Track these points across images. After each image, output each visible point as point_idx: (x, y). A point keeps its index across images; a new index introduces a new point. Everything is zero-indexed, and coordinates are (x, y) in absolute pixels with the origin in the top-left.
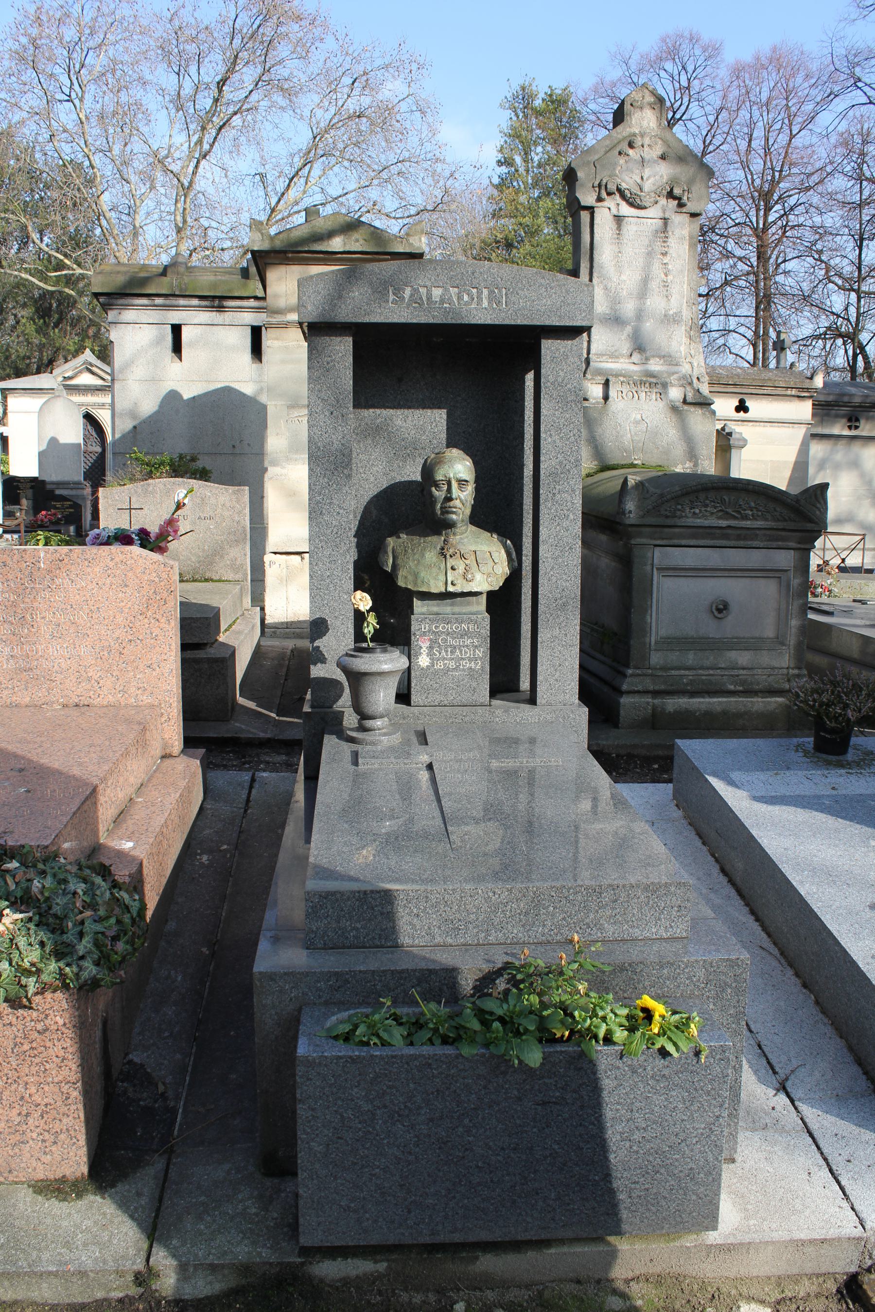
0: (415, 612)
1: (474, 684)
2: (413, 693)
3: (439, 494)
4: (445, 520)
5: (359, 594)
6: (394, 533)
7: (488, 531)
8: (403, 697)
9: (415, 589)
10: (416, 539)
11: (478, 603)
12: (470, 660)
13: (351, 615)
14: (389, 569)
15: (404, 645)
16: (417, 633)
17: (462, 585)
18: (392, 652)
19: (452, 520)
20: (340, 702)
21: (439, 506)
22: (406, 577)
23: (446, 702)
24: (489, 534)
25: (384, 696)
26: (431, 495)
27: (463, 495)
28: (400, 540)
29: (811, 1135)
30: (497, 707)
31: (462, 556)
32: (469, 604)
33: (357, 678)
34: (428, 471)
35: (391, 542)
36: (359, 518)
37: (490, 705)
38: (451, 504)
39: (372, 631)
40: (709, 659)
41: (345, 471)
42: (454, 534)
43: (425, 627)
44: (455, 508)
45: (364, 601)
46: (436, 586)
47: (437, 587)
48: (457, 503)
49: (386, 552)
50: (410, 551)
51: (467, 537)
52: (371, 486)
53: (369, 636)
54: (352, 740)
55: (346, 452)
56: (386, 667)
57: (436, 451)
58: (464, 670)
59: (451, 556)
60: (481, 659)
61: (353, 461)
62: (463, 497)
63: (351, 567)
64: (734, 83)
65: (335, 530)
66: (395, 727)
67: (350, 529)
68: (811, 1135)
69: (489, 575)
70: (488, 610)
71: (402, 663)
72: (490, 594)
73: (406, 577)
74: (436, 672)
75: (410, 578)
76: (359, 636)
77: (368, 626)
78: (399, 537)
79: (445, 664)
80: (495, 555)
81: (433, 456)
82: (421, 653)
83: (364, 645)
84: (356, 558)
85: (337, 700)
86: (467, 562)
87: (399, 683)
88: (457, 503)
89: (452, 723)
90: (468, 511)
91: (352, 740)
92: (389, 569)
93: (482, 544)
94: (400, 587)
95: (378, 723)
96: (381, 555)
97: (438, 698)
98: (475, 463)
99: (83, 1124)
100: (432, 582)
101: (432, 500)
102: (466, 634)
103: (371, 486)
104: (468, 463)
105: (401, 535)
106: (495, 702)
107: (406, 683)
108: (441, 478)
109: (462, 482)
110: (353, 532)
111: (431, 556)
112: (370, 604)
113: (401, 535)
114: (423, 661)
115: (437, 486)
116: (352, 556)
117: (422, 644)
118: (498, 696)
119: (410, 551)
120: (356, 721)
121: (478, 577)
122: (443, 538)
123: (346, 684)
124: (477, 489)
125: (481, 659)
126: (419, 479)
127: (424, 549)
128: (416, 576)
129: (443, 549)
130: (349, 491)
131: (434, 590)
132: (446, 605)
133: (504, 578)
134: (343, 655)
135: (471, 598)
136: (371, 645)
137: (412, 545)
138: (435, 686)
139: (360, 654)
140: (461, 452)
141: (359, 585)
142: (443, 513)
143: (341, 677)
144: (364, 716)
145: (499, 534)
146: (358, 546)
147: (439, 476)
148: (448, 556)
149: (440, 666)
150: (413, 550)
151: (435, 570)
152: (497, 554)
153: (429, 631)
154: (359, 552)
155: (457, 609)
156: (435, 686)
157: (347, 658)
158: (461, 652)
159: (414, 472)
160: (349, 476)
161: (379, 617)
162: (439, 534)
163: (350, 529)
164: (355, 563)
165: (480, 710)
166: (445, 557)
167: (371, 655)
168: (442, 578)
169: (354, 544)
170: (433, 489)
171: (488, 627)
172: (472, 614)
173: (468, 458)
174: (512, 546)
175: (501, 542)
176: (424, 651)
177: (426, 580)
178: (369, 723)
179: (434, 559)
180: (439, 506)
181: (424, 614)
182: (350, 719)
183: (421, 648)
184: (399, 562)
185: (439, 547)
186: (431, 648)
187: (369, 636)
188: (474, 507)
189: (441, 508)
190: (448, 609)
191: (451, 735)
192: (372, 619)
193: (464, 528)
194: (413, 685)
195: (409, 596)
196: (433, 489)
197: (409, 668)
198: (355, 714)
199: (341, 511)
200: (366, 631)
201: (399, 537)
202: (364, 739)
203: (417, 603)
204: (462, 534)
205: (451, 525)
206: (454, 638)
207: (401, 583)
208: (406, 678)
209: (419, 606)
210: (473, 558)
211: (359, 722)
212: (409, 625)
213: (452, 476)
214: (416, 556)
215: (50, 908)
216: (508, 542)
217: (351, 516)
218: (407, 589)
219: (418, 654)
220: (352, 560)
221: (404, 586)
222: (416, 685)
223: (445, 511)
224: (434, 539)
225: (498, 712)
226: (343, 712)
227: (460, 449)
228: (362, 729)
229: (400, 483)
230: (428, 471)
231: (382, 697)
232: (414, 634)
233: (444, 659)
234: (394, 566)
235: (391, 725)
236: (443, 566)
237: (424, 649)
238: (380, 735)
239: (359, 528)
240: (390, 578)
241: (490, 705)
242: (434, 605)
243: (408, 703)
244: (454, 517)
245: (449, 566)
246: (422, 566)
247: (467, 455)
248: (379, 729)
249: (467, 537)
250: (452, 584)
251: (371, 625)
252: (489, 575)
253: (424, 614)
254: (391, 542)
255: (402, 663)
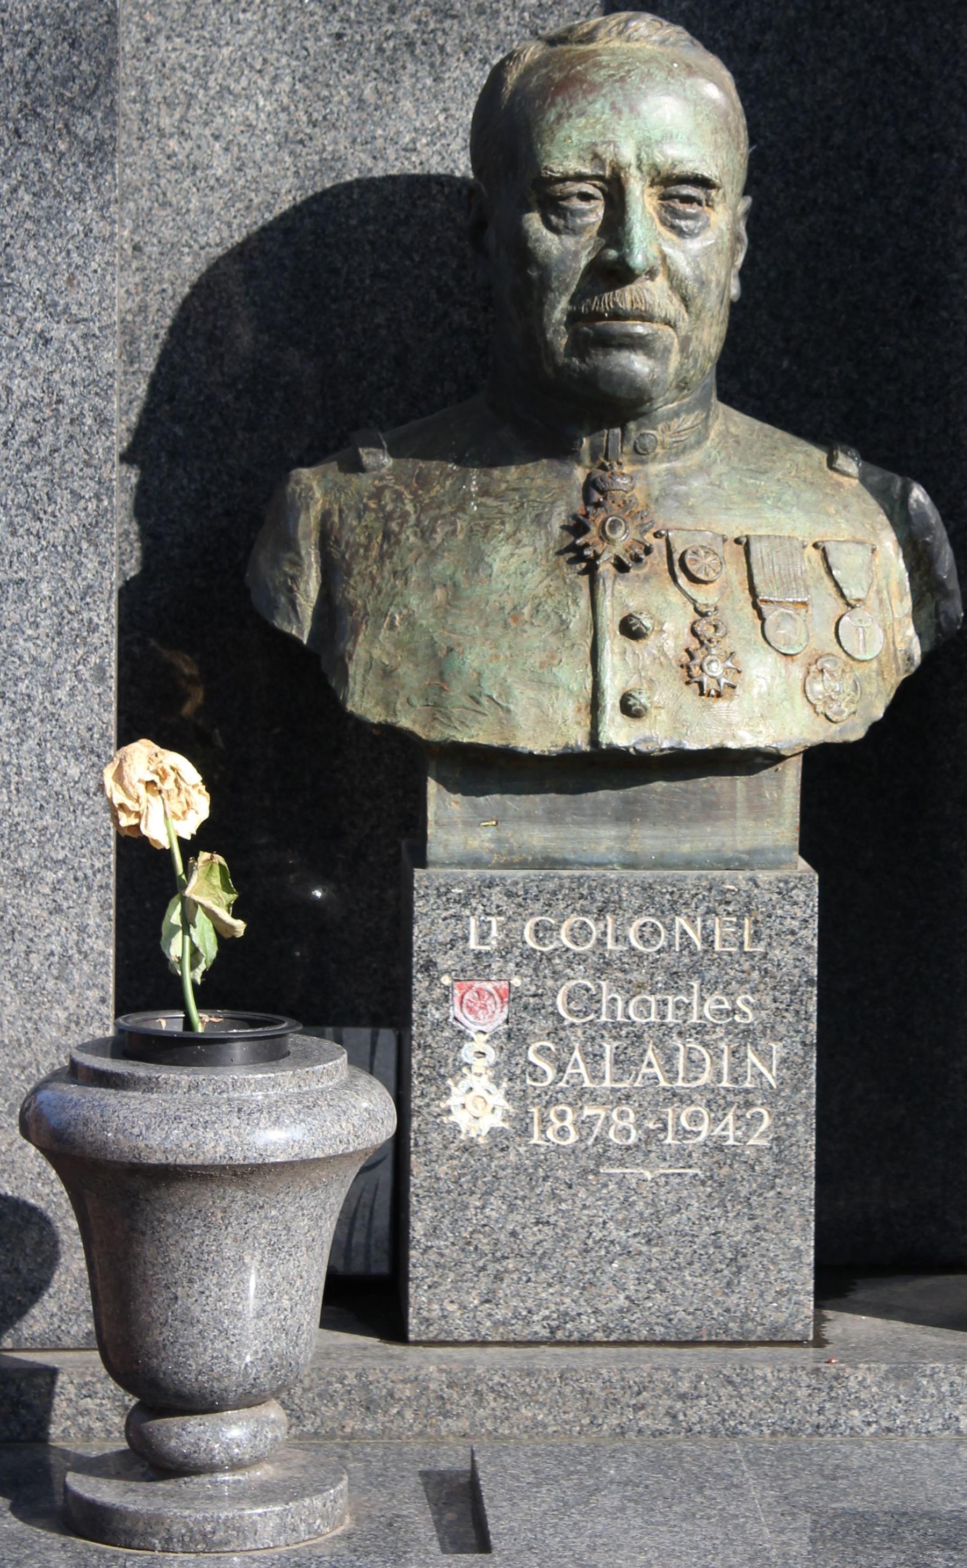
0: (434, 849)
1: (737, 1230)
2: (416, 1272)
3: (564, 248)
4: (590, 380)
5: (143, 756)
6: (334, 444)
7: (815, 436)
8: (367, 1292)
9: (435, 734)
10: (443, 476)
11: (758, 810)
12: (716, 1102)
13: (103, 864)
14: (302, 628)
15: (376, 1022)
16: (445, 961)
17: (677, 720)
18: (306, 1058)
19: (628, 379)
20: (38, 1320)
21: (560, 308)
22: (387, 673)
23: (588, 1324)
24: (819, 455)
25: (268, 1291)
26: (522, 251)
27: (685, 255)
28: (363, 482)
29: (752, 589)
30: (857, 1353)
31: (679, 567)
32: (710, 811)
33: (126, 1201)
34: (508, 126)
35: (314, 489)
36: (149, 364)
37: (819, 1342)
38: (626, 297)
39: (210, 949)
40: (562, 835)
41: (82, 126)
42: (640, 453)
43: (481, 931)
44: (646, 317)
45: (168, 795)
46: (544, 721)
47: (545, 723)
48: (654, 293)
49: (289, 543)
50: (410, 537)
51: (703, 469)
52: (215, 201)
53: (191, 976)
54: (93, 1523)
55: (86, 25)
56: (275, 1139)
57: (553, 25)
58: (683, 1156)
59: (621, 567)
60: (771, 1097)
61: (123, 72)
62: (683, 265)
63: (105, 616)
64: (394, 1378)
65: (26, 426)
66: (322, 1448)
67: (103, 421)
68: (752, 589)
69: (815, 665)
70: (809, 846)
71: (366, 1115)
72: (825, 766)
73: (387, 673)
74: (538, 1168)
75: (411, 675)
76: (142, 976)
77: (187, 923)
78: (356, 467)
79: (585, 1125)
80: (848, 563)
81: (533, 51)
82: (460, 1067)
83: (167, 1023)
84: (132, 569)
85: (22, 1311)
86: (704, 596)
87: (349, 1220)
88: (654, 293)
89: (622, 1432)
90: (710, 336)
91: (93, 1523)
92: (302, 628)
93: (779, 504)
94: (360, 724)
95: (233, 1432)
96: (262, 558)
97: (543, 1300)
98: (749, 90)
99: (412, 1300)
100: (522, 700)
101: (527, 276)
102: (695, 970)
103: (215, 201)
104: (712, 91)
105: (368, 456)
106: (848, 1326)
107: (383, 1221)
108: (573, 166)
109: (680, 191)
110: (119, 436)
111: (517, 563)
112: (853, 708)
113: (368, 456)
114: (473, 1105)
115: (553, 206)
116: (111, 558)
117: (466, 1016)
118: (861, 1295)
119: (410, 537)
120: (118, 1421)
121: (762, 672)
122: (580, 474)
123: (67, 1226)
124: (758, 224)
125: (771, 1097)
126: (462, 166)
127: (483, 528)
128: (440, 664)
129: (578, 527)
130: (101, 228)
131: (534, 740)
132: (597, 816)
133: (894, 680)
134: (55, 1076)
135: (720, 783)
136: (202, 1021)
137: (422, 509)
138: (531, 1236)
139: (141, 1070)
140: (676, 33)
141: (145, 712)
142: (580, 345)
143: (40, 1185)
144: (157, 1393)
145: (867, 456)
146: (146, 506)
147: (565, 156)
148: (606, 567)
149: (558, 1130)
150: (425, 534)
151: (536, 638)
152: (859, 556)
153: (505, 952)
154: (152, 539)
155: (649, 839)
156: (531, 1236)
157: (73, 1091)
158: (670, 1059)
159: (437, 134)
160: (100, 152)
161: (237, 877)
162: (563, 451)
163: (103, 421)
164: (130, 595)
165: (764, 1365)
166: (591, 570)
167: (201, 1075)
168: (573, 676)
169: (122, 502)
170: (534, 222)
171: (810, 935)
172: (727, 864)
173: (713, 63)
174: (934, 517)
175: (881, 494)
176: (480, 1054)
177: (490, 688)
178: (185, 1434)
179: (535, 581)
180: (560, 308)
181: (477, 863)
182: (87, 1412)
183: (462, 1036)
184: (356, 591)
185: (558, 520)
186: (513, 1037)
187: (191, 976)
188: (740, 315)
189: (573, 318)
190: (604, 839)
191: (609, 1500)
192: (207, 889)
193: (688, 421)
194: (418, 1229)
195: (401, 768)
196: (534, 222)
197: (400, 1144)
198: (112, 1385)
199: (58, 331)
200: (176, 948)
201: (356, 467)
202: (156, 1520)
203: (443, 806)
204: (680, 450)
205: (623, 407)
206: (632, 990)
207: (363, 702)
208: (384, 1197)
209: (454, 823)
210: (735, 573)
211: (133, 1430)
212: (403, 920)
213: (628, 154)
214: (443, 566)
215: (535, 970)
216: (918, 494)
217: (110, 357)
218: (390, 732)
219: (447, 1070)
220: (112, 580)
221: (374, 714)
222: (434, 1232)
223: (597, 332)
224: (531, 476)
225: (862, 1377)
226: (52, 1373)
227: (673, 19)
228: (149, 1461)
229: (367, 185)
230: (508, 126)
231: (254, 1294)
232: (429, 965)
233: (582, 1095)
234: (330, 611)
235: (302, 1440)
236: (578, 615)
237: (480, 1043)
238: (241, 1495)
239: (149, 413)
240: (312, 671)
241: (819, 1342)
242: (529, 818)
243: (394, 1331)
244: (639, 364)
245: (610, 617)
246: (477, 618)
247: (711, 46)
248: (237, 1465)
249: (703, 469)
250: (628, 708)
251: (204, 916)
252: (815, 665)
253: (477, 863)
254: (314, 489)
255: (366, 1115)
